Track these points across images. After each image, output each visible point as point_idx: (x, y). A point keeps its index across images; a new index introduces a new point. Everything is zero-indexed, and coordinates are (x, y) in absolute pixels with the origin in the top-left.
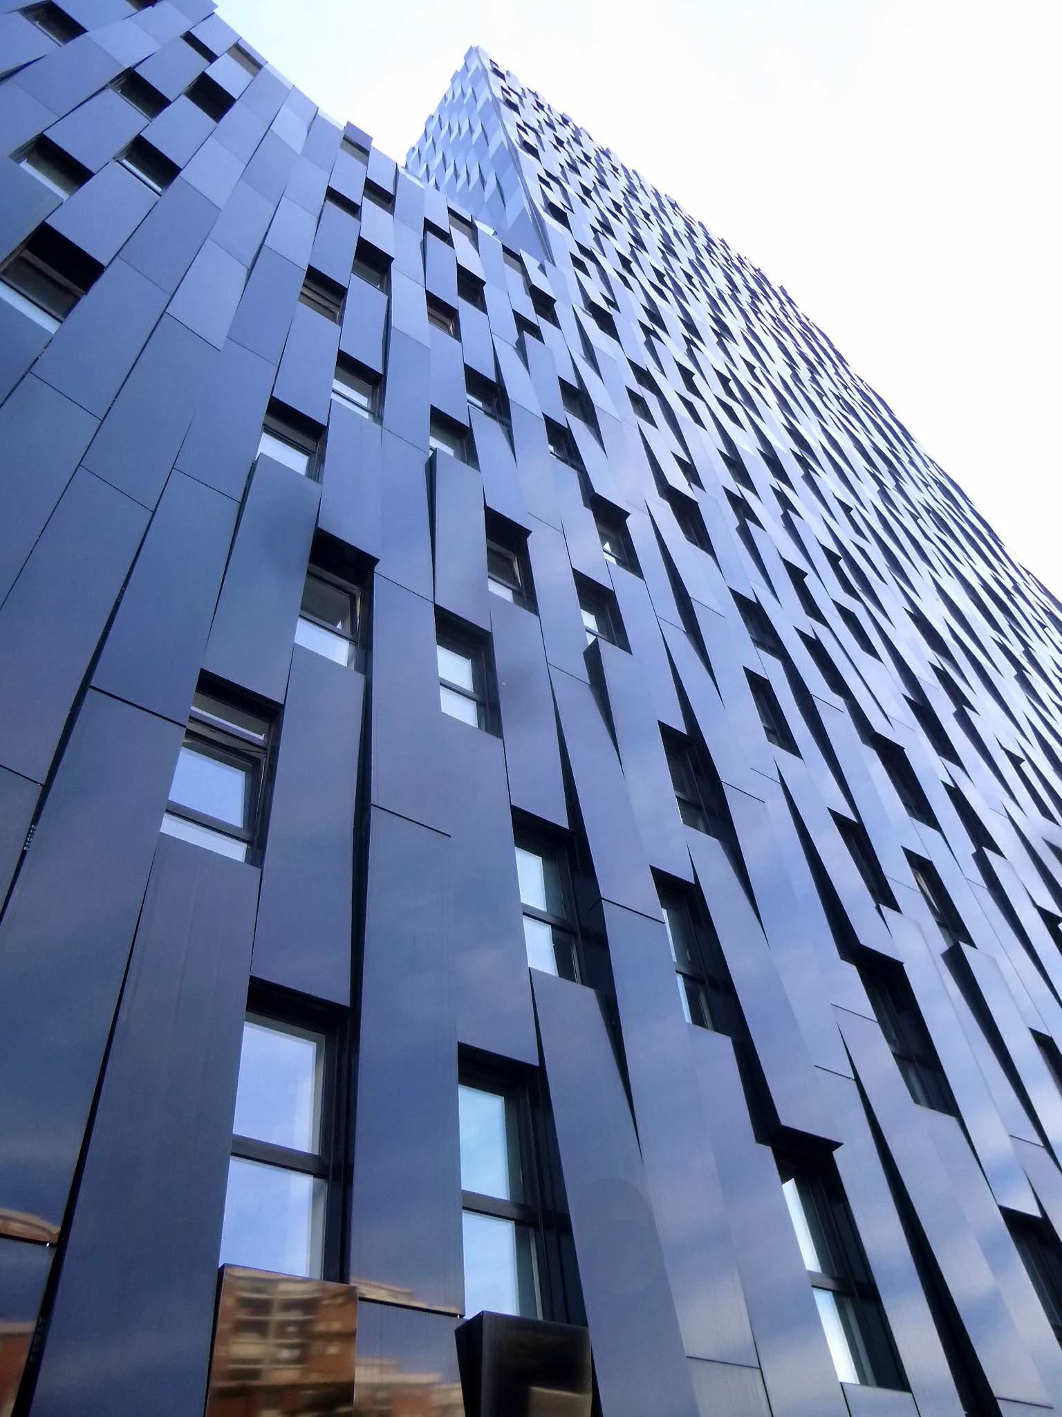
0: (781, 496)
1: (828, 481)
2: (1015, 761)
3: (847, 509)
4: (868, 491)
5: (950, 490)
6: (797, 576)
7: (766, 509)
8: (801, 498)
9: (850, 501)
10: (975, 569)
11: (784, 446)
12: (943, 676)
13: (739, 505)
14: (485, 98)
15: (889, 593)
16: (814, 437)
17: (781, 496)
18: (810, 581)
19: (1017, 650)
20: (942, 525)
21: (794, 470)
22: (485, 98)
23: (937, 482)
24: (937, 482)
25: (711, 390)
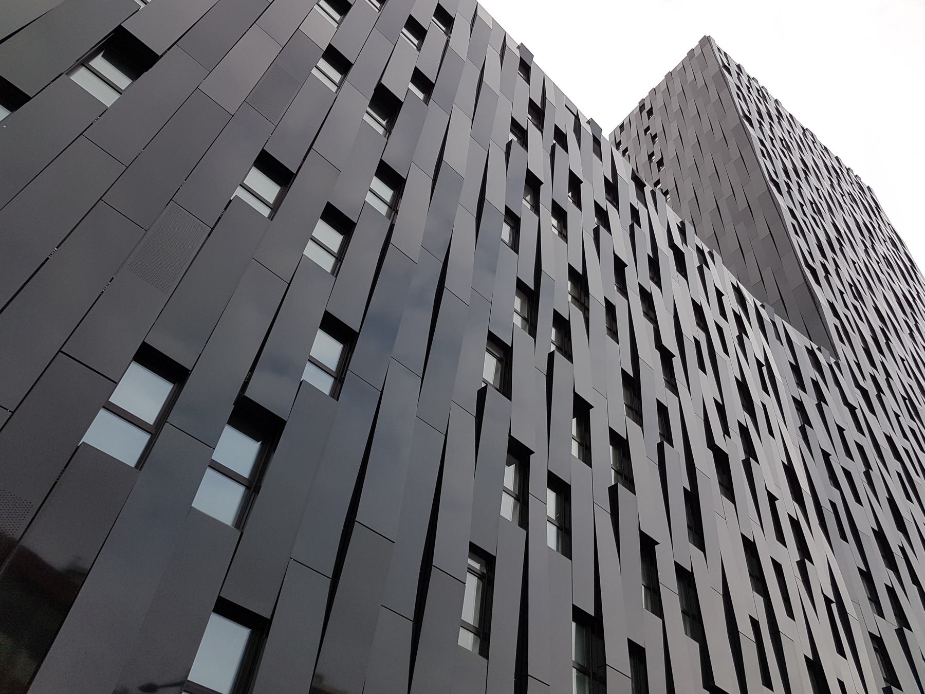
0: (798, 183)
1: (812, 179)
2: (903, 360)
3: (817, 190)
4: (827, 184)
5: (896, 242)
6: (802, 206)
7: (794, 187)
8: (804, 184)
9: (819, 186)
10: (862, 217)
11: (800, 166)
12: (882, 330)
13: (787, 184)
14: (708, 89)
15: (867, 297)
16: (810, 163)
17: (798, 183)
18: (804, 207)
19: (912, 324)
20: (889, 265)
21: (802, 175)
22: (708, 89)
23: (891, 239)
24: (891, 239)
25: (778, 144)
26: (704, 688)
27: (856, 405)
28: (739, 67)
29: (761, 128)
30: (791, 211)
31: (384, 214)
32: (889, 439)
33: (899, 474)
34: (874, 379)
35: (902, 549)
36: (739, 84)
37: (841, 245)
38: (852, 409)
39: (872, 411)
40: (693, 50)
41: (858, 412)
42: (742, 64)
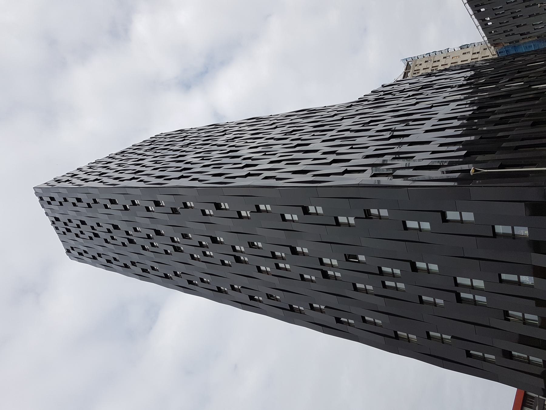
13: (187, 163)
26: (76, 253)
27: (343, 169)
28: (78, 169)
29: (147, 167)
30: (204, 166)
31: (417, 263)
32: (272, 162)
33: (287, 164)
34: (292, 140)
35: (314, 175)
36: (114, 170)
37: (184, 151)
38: (249, 175)
39: (348, 160)
40: (46, 213)
41: (349, 169)
42: (78, 167)
